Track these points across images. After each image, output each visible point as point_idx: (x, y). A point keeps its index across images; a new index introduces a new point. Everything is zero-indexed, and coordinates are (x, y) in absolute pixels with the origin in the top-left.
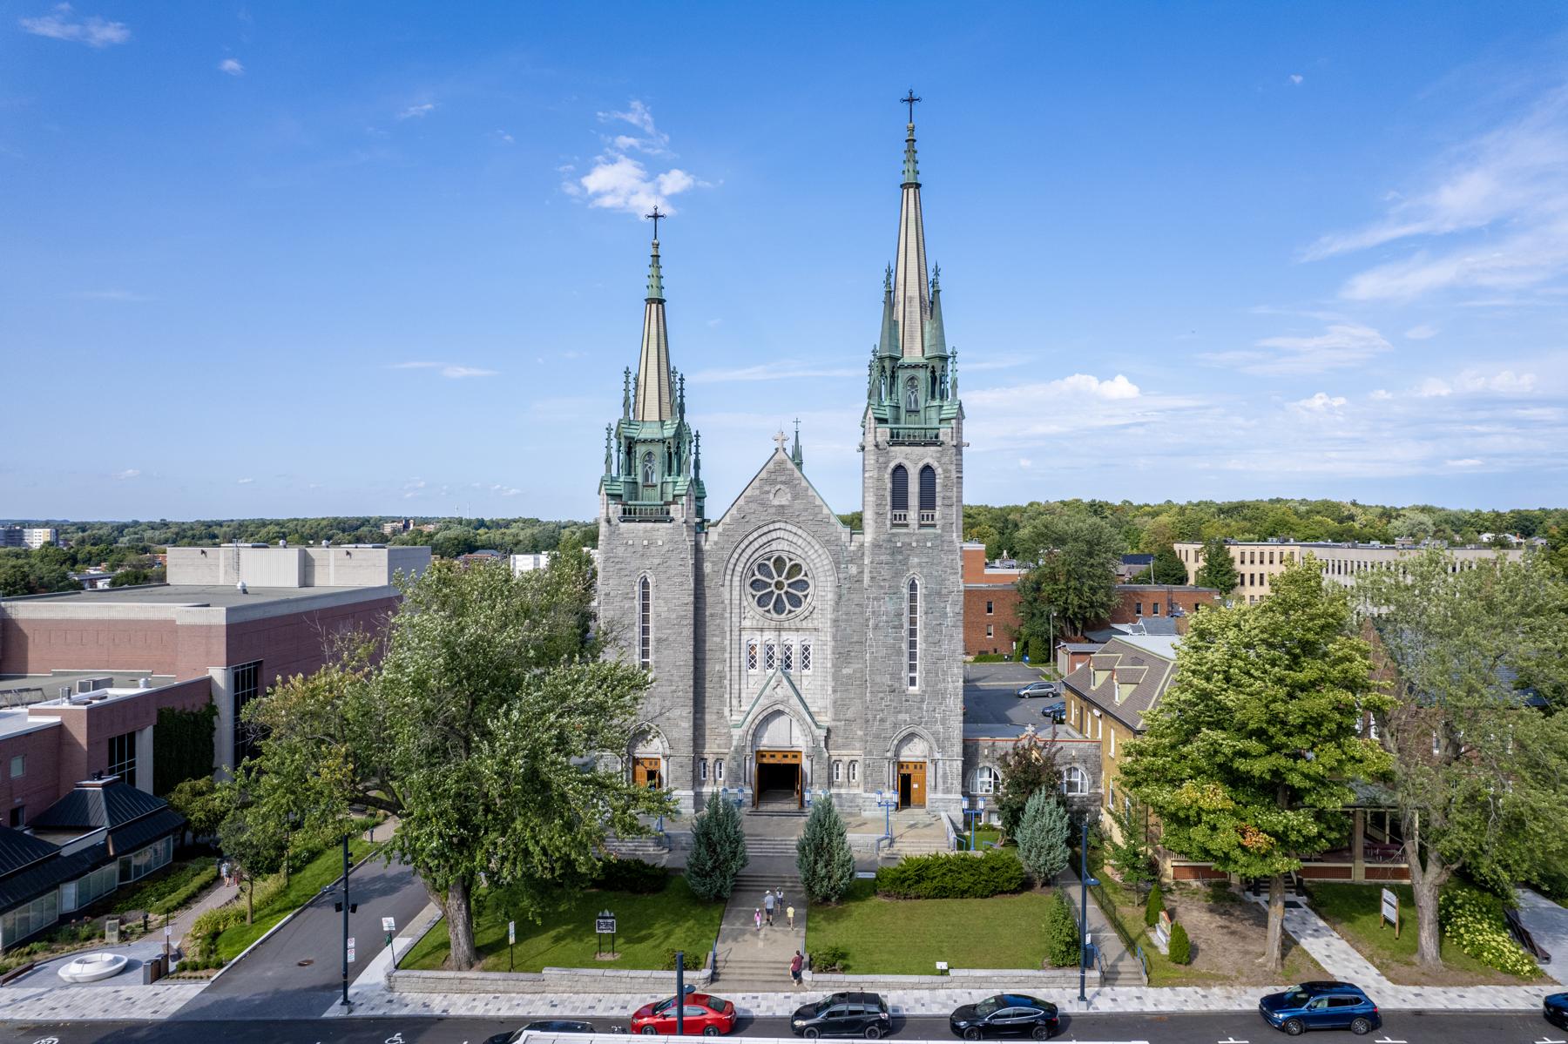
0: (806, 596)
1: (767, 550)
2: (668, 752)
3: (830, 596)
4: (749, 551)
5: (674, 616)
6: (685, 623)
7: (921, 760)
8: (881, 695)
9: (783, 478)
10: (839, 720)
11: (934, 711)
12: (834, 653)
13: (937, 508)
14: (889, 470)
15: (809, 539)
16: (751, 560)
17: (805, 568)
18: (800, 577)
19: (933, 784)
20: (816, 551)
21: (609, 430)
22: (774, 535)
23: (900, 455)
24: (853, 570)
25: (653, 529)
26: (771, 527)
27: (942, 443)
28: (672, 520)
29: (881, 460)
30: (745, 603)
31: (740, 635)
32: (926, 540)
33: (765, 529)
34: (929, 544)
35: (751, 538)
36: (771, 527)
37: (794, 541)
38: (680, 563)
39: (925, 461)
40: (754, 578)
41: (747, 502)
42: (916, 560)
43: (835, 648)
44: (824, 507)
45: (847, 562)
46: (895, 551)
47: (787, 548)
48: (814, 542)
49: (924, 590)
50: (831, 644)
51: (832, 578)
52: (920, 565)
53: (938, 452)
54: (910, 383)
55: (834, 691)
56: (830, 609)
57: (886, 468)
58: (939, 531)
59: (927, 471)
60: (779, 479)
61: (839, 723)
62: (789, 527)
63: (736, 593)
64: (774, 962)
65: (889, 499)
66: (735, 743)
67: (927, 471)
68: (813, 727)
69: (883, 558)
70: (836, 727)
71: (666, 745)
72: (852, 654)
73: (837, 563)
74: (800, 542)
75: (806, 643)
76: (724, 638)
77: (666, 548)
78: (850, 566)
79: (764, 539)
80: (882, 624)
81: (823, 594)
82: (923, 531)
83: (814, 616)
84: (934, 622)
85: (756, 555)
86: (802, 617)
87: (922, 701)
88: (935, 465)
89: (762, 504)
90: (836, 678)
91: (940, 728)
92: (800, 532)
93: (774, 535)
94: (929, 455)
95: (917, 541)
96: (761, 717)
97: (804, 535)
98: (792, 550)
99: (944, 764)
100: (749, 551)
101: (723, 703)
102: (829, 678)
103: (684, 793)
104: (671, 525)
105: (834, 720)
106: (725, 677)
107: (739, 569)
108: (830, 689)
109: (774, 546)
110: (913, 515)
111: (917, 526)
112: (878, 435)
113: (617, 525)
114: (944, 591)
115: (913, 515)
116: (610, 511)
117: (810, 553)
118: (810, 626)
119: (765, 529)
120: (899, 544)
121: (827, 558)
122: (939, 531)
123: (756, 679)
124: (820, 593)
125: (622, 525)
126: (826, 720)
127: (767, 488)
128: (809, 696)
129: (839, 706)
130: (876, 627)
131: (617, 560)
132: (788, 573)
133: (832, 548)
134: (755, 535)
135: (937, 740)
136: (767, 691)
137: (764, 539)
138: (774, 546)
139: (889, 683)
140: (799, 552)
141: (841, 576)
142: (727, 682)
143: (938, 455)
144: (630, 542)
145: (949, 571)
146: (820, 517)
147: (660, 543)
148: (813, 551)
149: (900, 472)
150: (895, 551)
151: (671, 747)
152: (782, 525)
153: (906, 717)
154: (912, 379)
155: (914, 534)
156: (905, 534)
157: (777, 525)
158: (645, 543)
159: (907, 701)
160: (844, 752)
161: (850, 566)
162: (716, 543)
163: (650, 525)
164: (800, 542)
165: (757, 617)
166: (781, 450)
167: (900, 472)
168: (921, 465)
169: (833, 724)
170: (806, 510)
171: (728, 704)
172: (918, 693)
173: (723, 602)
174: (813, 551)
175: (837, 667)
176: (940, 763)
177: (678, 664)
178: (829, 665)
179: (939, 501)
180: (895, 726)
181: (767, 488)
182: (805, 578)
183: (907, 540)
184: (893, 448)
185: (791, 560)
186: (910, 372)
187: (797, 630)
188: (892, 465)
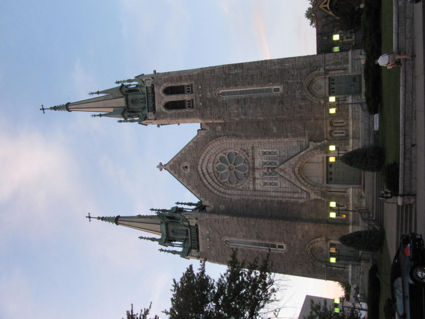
0: (236, 154)
1: (213, 174)
2: (324, 239)
3: (233, 140)
4: (214, 184)
5: (244, 228)
6: (248, 222)
7: (327, 81)
8: (284, 109)
9: (177, 166)
10: (305, 133)
11: (293, 75)
12: (265, 138)
13: (183, 84)
14: (167, 111)
15: (205, 152)
16: (218, 183)
17: (221, 155)
18: (226, 157)
19: (342, 71)
20: (211, 149)
21: (161, 250)
22: (205, 171)
23: (159, 106)
24: (219, 128)
25: (202, 235)
26: (201, 172)
27: (153, 85)
28: (196, 225)
29: (162, 116)
30: (241, 187)
31: (258, 191)
32: (198, 89)
33: (202, 176)
34: (200, 87)
35: (206, 183)
36: (201, 172)
37: (207, 160)
38: (217, 223)
39: (161, 93)
40: (228, 182)
41: (190, 185)
42: (209, 94)
43: (262, 137)
44: (189, 144)
45: (216, 132)
46: (205, 106)
47: (211, 164)
48: (207, 150)
49: (224, 88)
50: (260, 140)
51: (224, 140)
52: (210, 91)
53: (156, 86)
54: (134, 103)
55: (287, 137)
56: (241, 141)
57: (165, 113)
58: (193, 82)
59: (168, 91)
60: (178, 168)
61: (307, 134)
62: (200, 163)
63: (235, 192)
64: (373, 187)
65: (180, 111)
66: (319, 198)
67: (168, 91)
68: (308, 150)
69: (208, 112)
70: (309, 135)
71: (319, 239)
72: (265, 127)
73: (217, 137)
74: (207, 157)
75: (261, 153)
76: (259, 200)
77: (210, 230)
78: (217, 130)
79: (207, 176)
80: (243, 111)
81: (233, 144)
82: (194, 91)
83: (246, 149)
84: (241, 80)
85: (216, 180)
86: (247, 156)
87: (287, 83)
88: (162, 88)
89: (190, 177)
90: (278, 136)
91: (304, 71)
92: (202, 158)
93: (205, 171)
94: (159, 91)
95: (199, 94)
96: (303, 181)
97: (203, 155)
98: (212, 161)
99: (328, 65)
100: (214, 184)
101: (297, 203)
102: (279, 140)
103: (360, 229)
104: (199, 226)
105: (305, 135)
106: (281, 201)
107: (223, 190)
108: (286, 140)
109: (211, 171)
110: (186, 97)
111: (192, 95)
112: (151, 118)
113: (201, 253)
114: (224, 76)
115: (186, 97)
116: (195, 255)
117: (213, 152)
118: (251, 151)
119: (202, 176)
120: (201, 104)
121: (214, 142)
122: (193, 82)
123: (282, 183)
124: (233, 146)
125: (201, 249)
126: (304, 140)
127: (182, 174)
128: (291, 152)
129: (296, 134)
130: (245, 114)
131: (217, 255)
132: (225, 163)
133: (209, 139)
134: (205, 181)
135: (312, 71)
136: (287, 177)
137: (207, 176)
138: (211, 171)
139: (277, 104)
140: (213, 158)
141: (222, 134)
142: (284, 200)
143: (158, 86)
144: (208, 247)
145: (213, 75)
146: (194, 147)
147: (208, 232)
148: (212, 151)
149: (169, 106)
150: (205, 106)
151: (320, 236)
152: (199, 167)
153: (298, 92)
154: (132, 102)
155: (196, 96)
156: (196, 101)
157: (200, 169)
158: (208, 240)
159: (287, 93)
160: (325, 130)
161: (217, 130)
162: (210, 202)
163: (200, 236)
164: (207, 157)
165: (248, 181)
166: (166, 167)
167: (169, 106)
168: (163, 95)
169: (307, 137)
170: (191, 154)
171: (297, 200)
172: (282, 86)
173: (240, 200)
174: (212, 151)
175: (273, 136)
176: (327, 68)
177: (270, 228)
178: (272, 140)
179: (179, 84)
180: (304, 99)
181: (182, 174)
182: (227, 154)
183: (199, 100)
184: (157, 110)
185: (218, 162)
186: (130, 103)
187: (253, 159)
188: (164, 110)
